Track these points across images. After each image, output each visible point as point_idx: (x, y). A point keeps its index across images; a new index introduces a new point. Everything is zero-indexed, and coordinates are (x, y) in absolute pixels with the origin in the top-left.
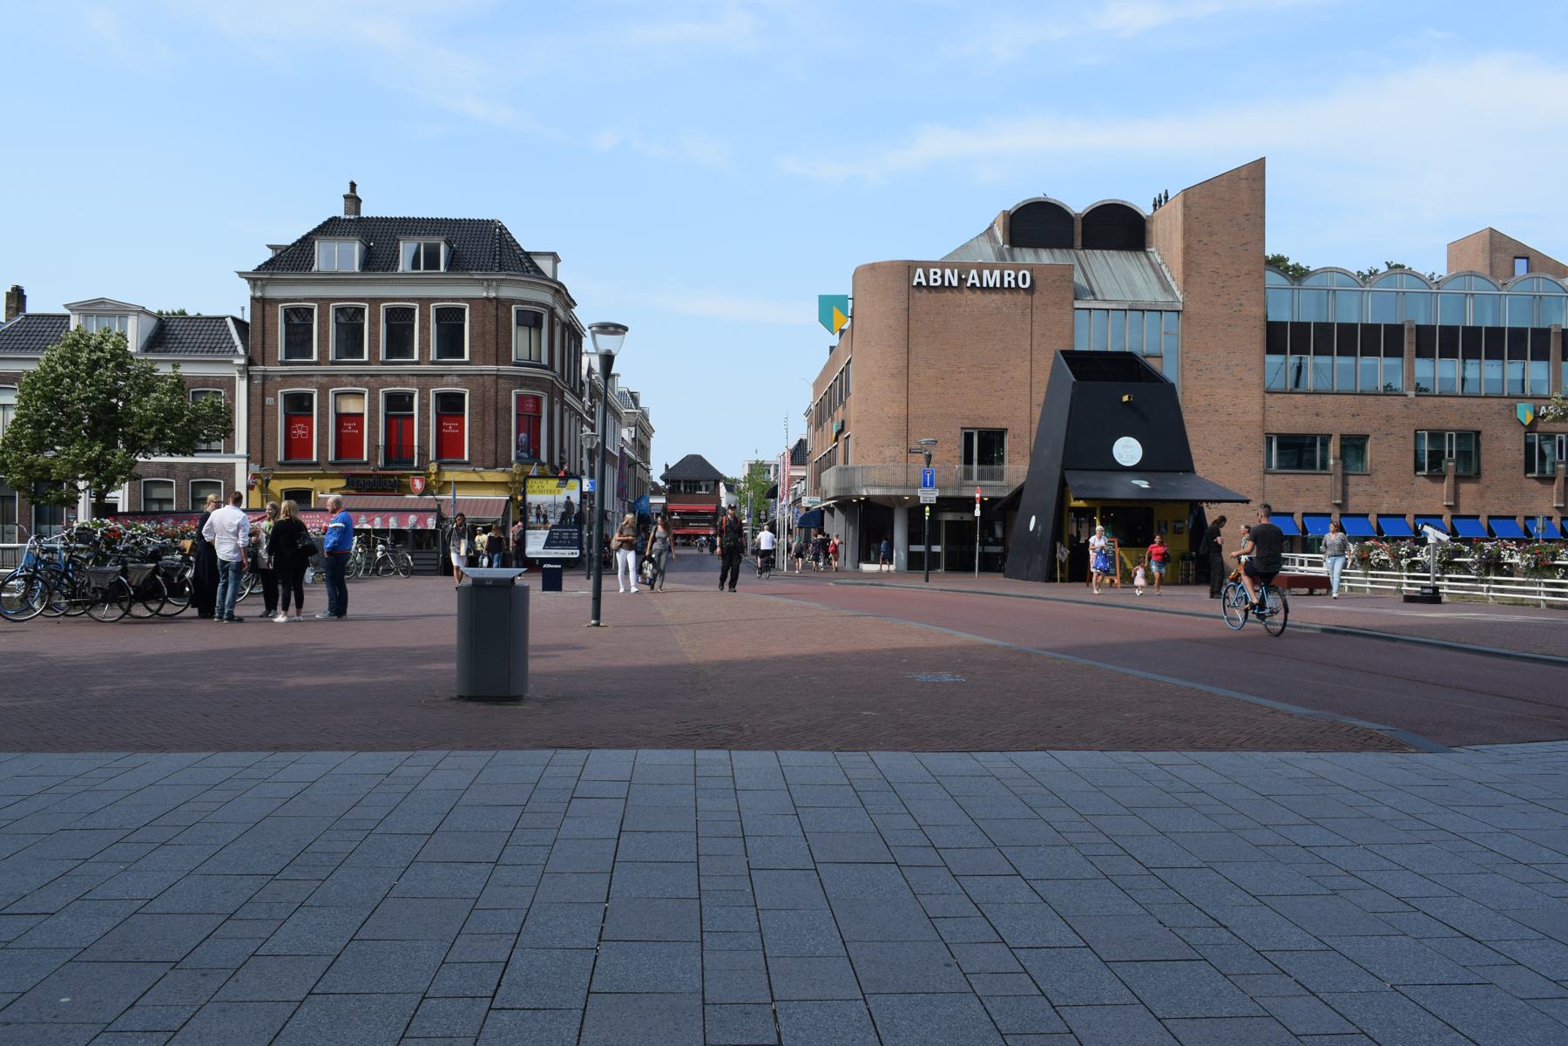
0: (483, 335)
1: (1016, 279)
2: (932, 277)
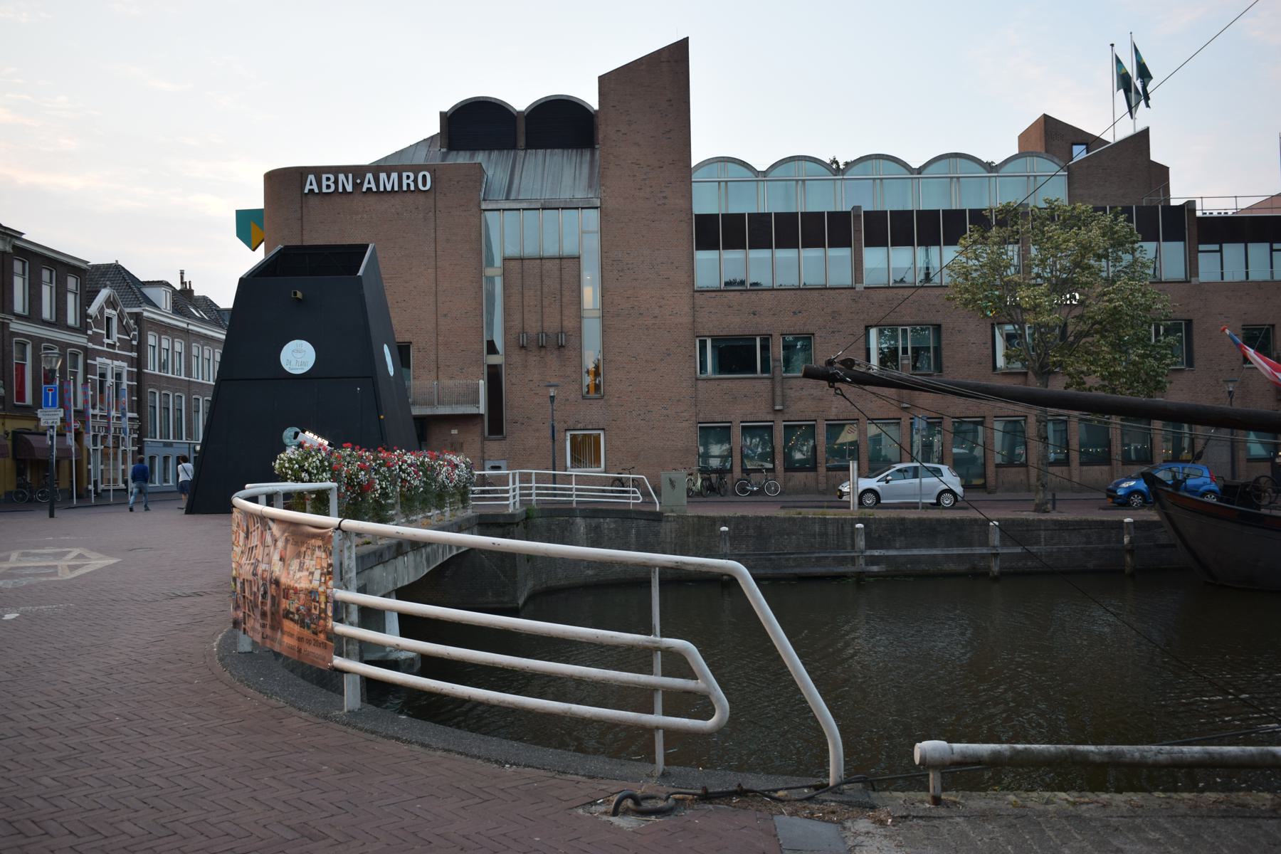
1: (415, 181)
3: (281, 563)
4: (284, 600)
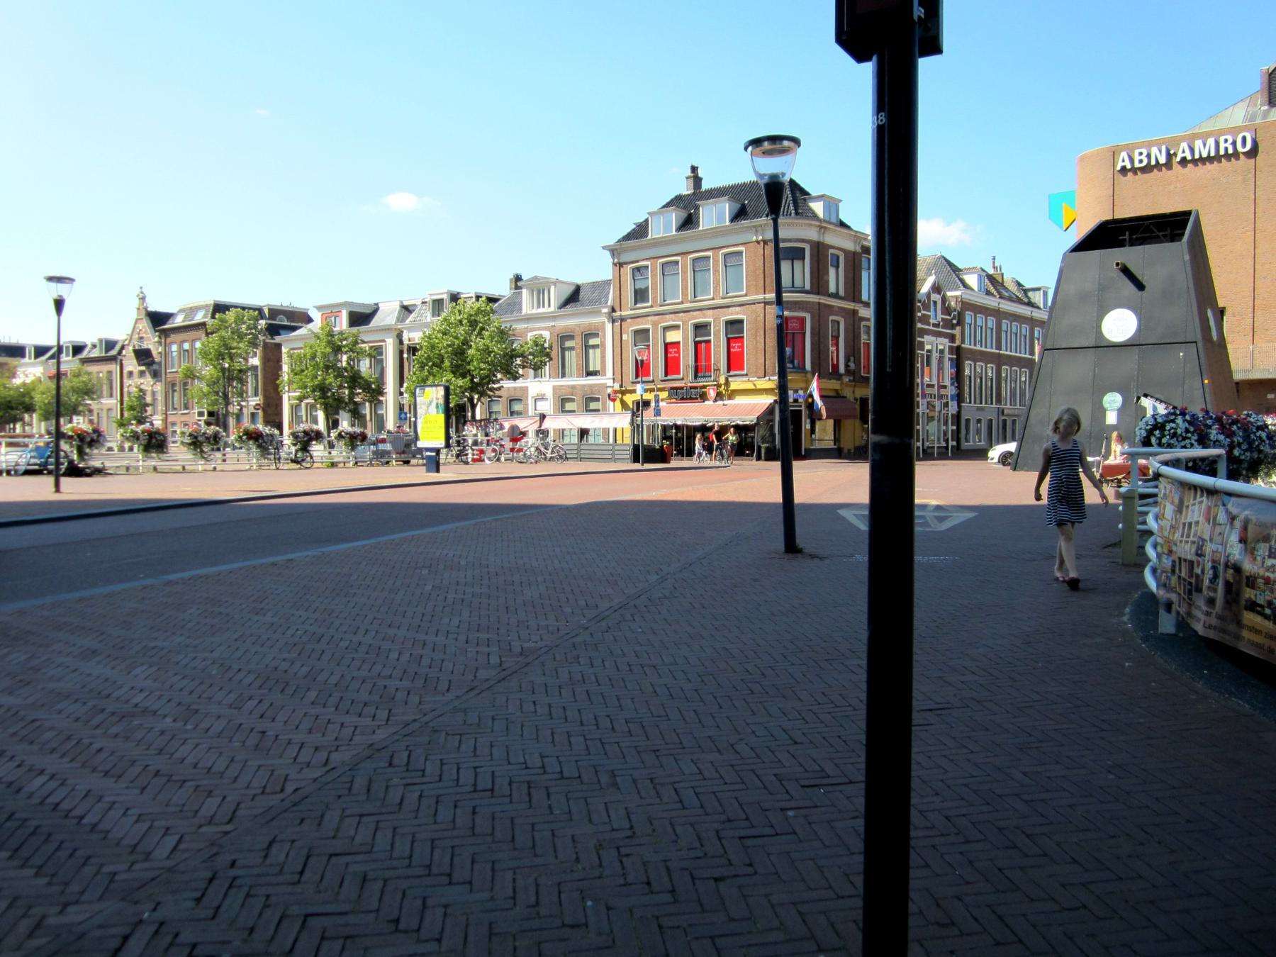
0: (755, 271)
1: (1234, 143)
2: (1137, 158)
3: (1240, 545)
4: (1248, 589)
